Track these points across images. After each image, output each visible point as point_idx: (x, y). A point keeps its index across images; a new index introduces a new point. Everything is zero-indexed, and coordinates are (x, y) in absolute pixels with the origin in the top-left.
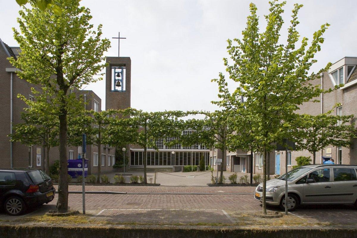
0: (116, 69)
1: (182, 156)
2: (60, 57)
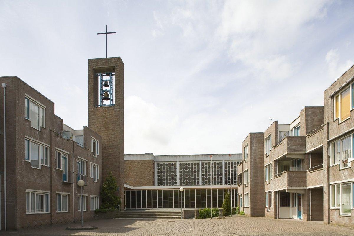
0: (103, 77)
1: (200, 195)
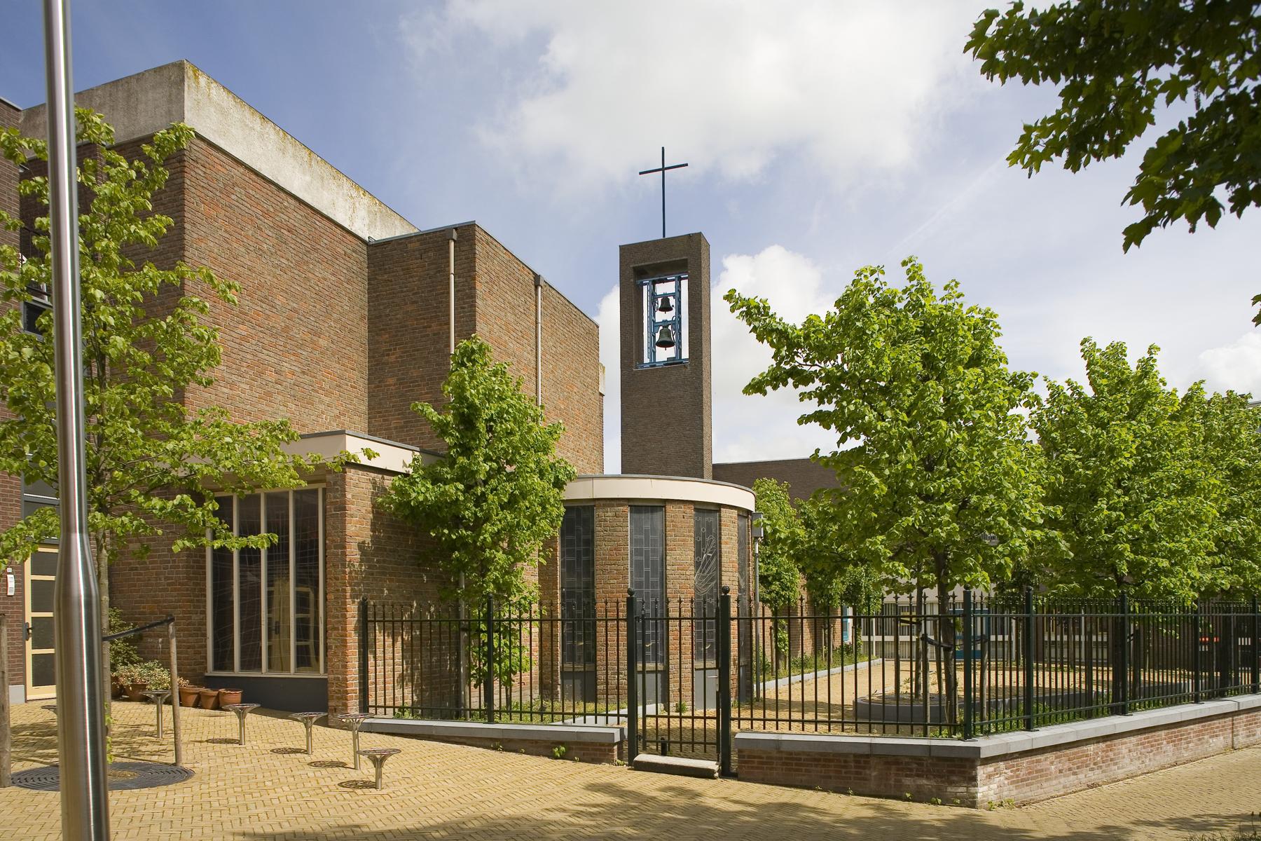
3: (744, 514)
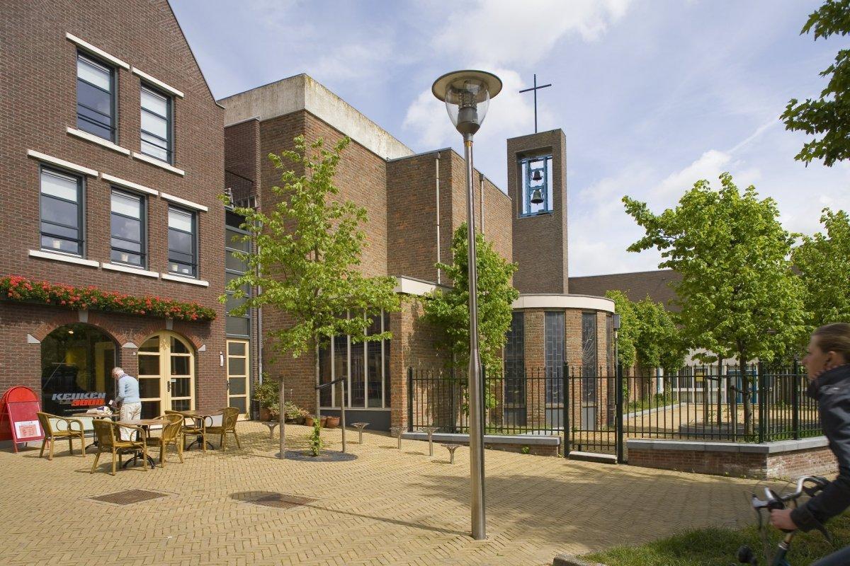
2: (663, 227)
3: (610, 314)
